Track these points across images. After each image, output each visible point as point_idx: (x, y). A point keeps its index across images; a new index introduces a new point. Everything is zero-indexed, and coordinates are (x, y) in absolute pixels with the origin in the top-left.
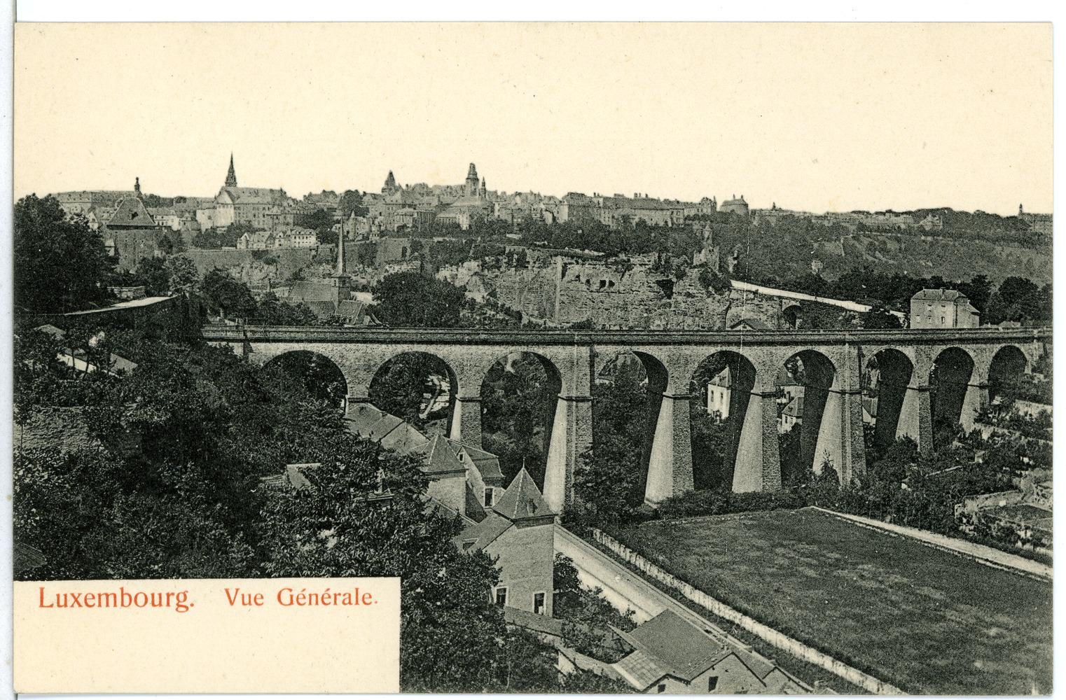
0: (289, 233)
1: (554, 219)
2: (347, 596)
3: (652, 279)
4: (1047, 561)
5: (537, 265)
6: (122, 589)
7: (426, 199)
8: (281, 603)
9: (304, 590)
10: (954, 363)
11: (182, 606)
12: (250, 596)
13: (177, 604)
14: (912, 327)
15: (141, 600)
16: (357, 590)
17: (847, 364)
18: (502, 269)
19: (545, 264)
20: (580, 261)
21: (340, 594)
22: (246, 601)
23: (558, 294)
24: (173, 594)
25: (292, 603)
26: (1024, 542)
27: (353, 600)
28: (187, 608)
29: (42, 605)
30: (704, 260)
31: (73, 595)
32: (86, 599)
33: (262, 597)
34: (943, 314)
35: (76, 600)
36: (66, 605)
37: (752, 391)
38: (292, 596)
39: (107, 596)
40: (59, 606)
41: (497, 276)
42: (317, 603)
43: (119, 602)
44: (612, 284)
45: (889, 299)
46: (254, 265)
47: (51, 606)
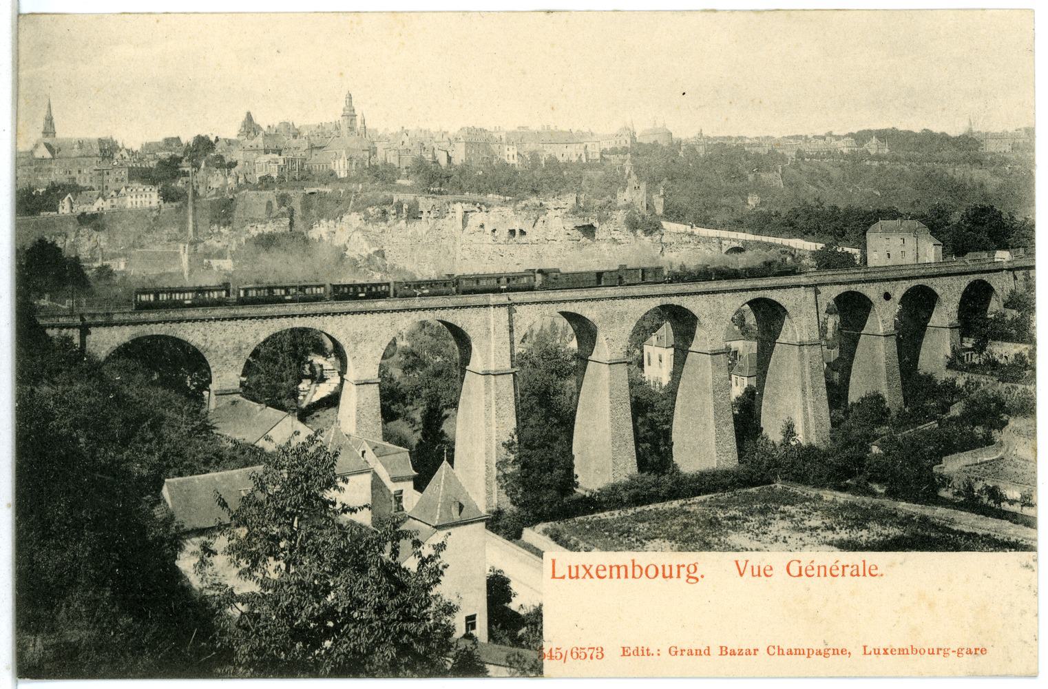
0: (123, 191)
1: (449, 159)
2: (855, 567)
3: (570, 226)
4: (1030, 523)
5: (432, 215)
6: (633, 561)
7: (294, 142)
8: (789, 574)
9: (813, 562)
10: (919, 303)
11: (692, 578)
12: (759, 567)
13: (688, 576)
14: (870, 264)
15: (652, 572)
16: (864, 561)
17: (806, 315)
18: (391, 221)
19: (441, 214)
20: (484, 208)
21: (847, 566)
22: (756, 572)
23: (458, 249)
24: (684, 566)
25: (800, 575)
26: (1012, 502)
27: (861, 572)
28: (697, 579)
29: (554, 577)
30: (629, 200)
31: (584, 566)
32: (597, 570)
33: (771, 569)
34: (898, 249)
35: (588, 571)
36: (577, 577)
37: (690, 349)
38: (800, 568)
39: (618, 567)
40: (571, 577)
41: (383, 231)
42: (825, 575)
43: (630, 574)
44: (523, 233)
45: (840, 235)
46: (81, 232)
47: (563, 577)
